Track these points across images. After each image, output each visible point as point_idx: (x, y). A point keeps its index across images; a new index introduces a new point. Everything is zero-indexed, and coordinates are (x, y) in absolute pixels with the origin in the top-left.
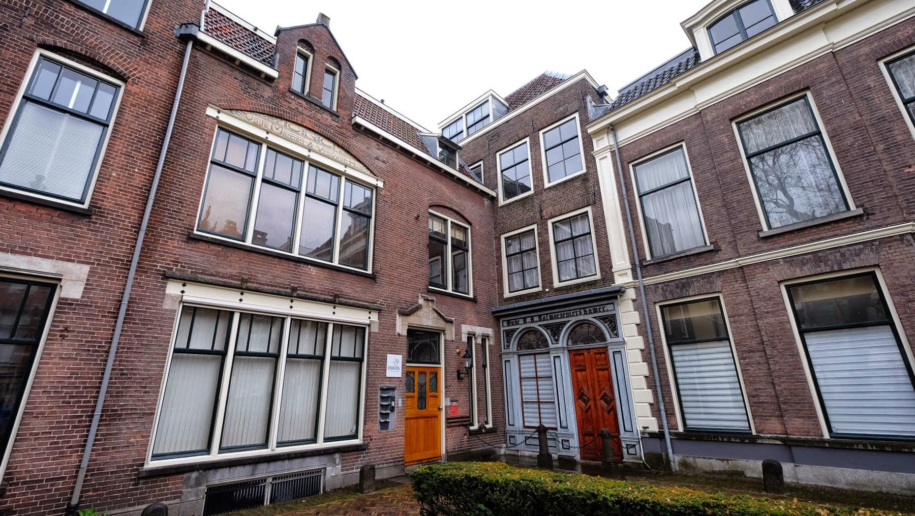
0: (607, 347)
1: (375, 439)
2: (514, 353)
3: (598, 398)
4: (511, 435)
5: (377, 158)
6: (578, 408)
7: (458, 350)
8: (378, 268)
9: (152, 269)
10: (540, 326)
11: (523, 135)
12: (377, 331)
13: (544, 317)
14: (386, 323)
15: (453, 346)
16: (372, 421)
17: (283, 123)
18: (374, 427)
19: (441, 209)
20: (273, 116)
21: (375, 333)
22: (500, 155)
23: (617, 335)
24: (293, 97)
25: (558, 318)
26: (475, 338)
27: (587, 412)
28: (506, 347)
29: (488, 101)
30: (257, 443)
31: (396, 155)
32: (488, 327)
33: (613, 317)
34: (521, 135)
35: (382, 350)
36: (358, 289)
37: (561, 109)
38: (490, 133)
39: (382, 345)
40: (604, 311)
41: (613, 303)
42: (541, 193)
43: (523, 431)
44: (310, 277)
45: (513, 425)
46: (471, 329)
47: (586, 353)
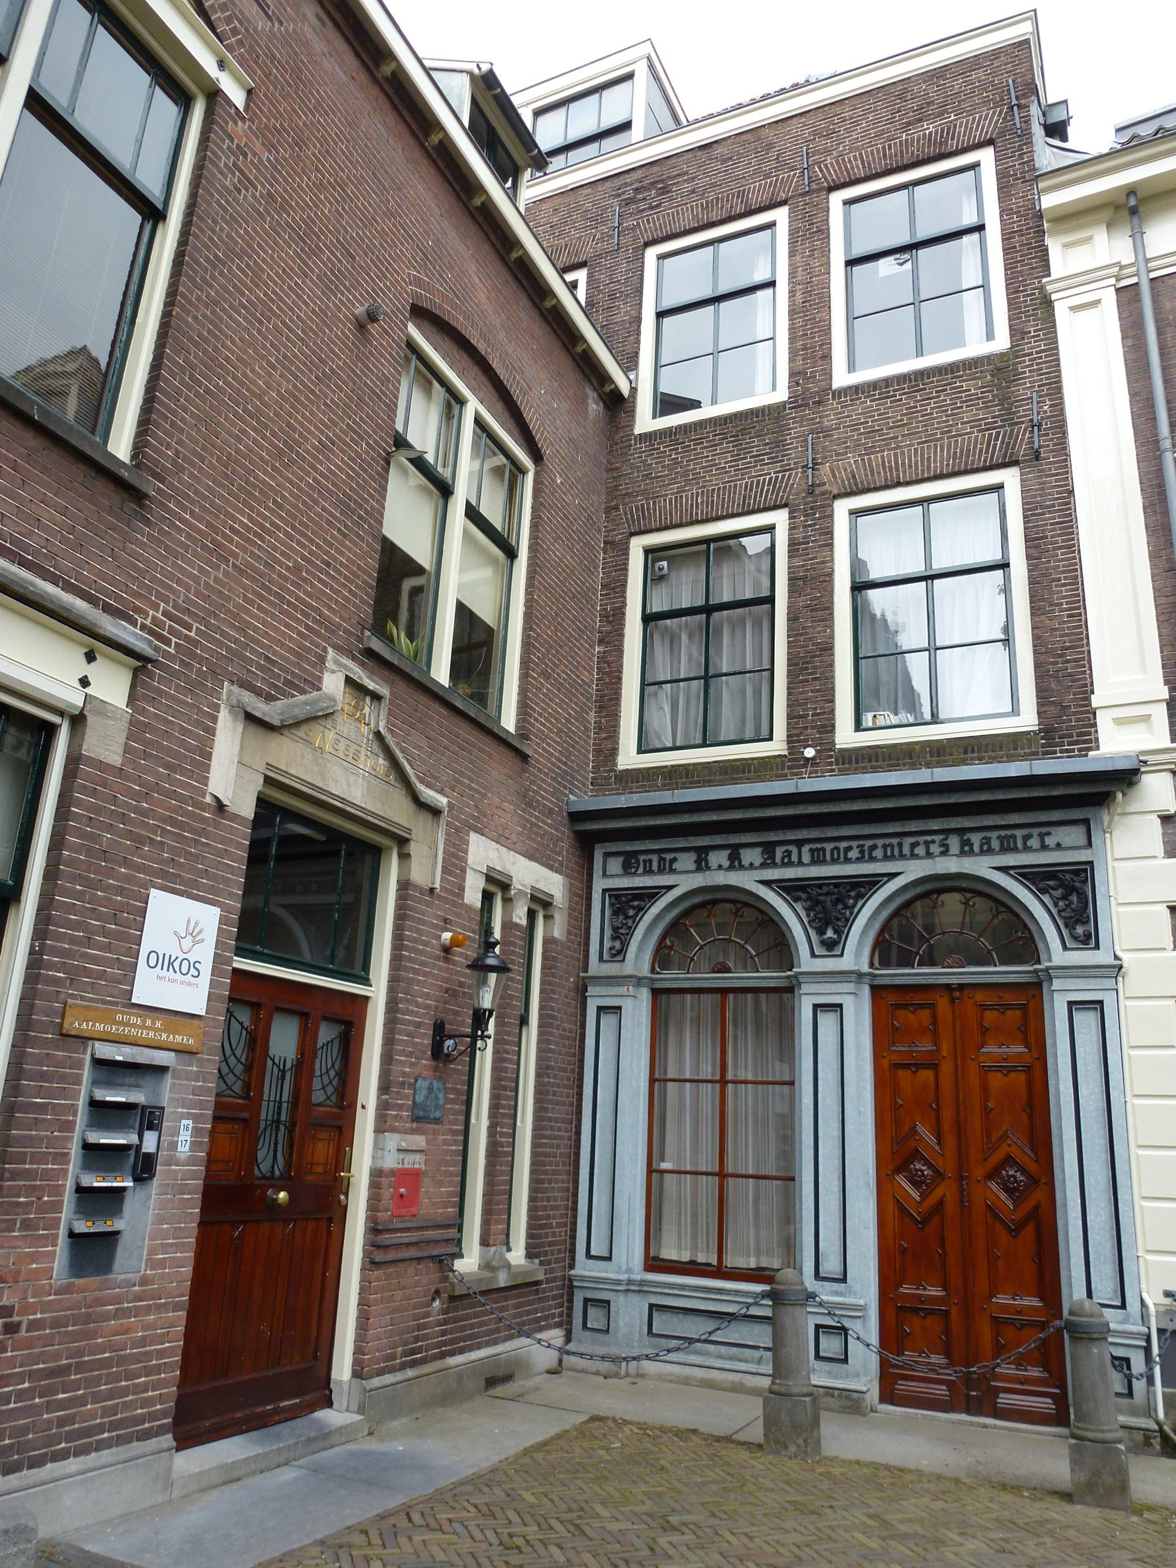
0: (1039, 985)
1: (34, 1325)
2: (639, 981)
3: (978, 1172)
4: (590, 1295)
6: (890, 1206)
7: (447, 936)
8: (164, 453)
10: (767, 883)
11: (765, 198)
12: (116, 760)
13: (789, 854)
15: (431, 913)
16: (27, 1225)
18: (33, 1258)
21: (102, 765)
22: (662, 257)
23: (1090, 940)
25: (848, 861)
26: (507, 901)
27: (925, 1221)
28: (606, 957)
29: (630, 76)
31: (317, 16)
32: (551, 868)
33: (1076, 873)
34: (757, 192)
35: (126, 863)
37: (929, 128)
38: (628, 179)
39: (130, 835)
40: (1044, 847)
41: (1086, 822)
42: (819, 403)
43: (643, 1283)
45: (609, 1259)
46: (500, 858)
47: (943, 1004)
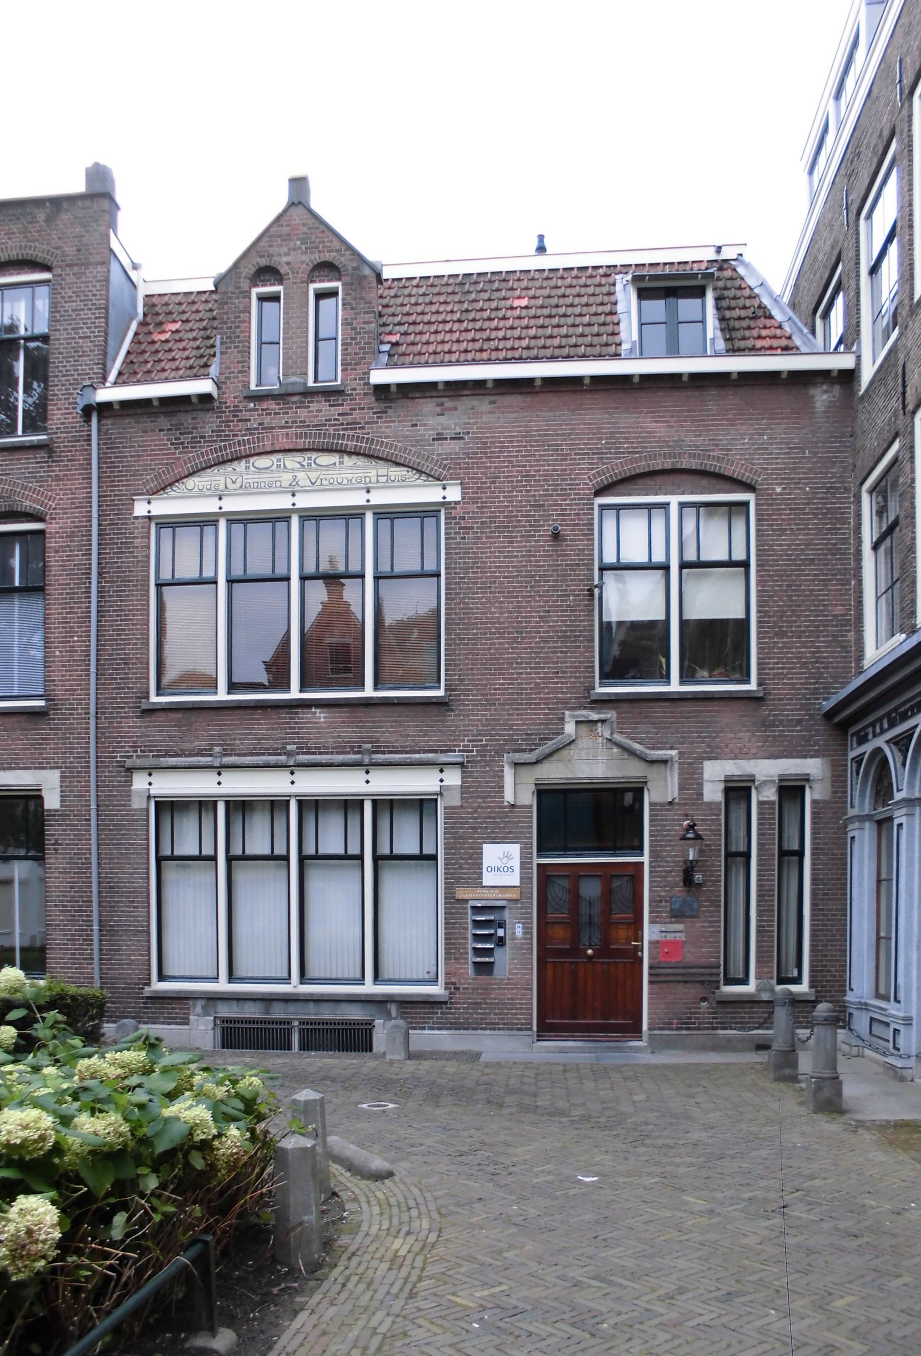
5: (440, 438)
9: (113, 762)
14: (478, 786)
17: (241, 466)
18: (461, 968)
19: (641, 483)
20: (224, 462)
24: (252, 405)
30: (279, 975)
32: (805, 757)
36: (411, 731)
44: (317, 728)
